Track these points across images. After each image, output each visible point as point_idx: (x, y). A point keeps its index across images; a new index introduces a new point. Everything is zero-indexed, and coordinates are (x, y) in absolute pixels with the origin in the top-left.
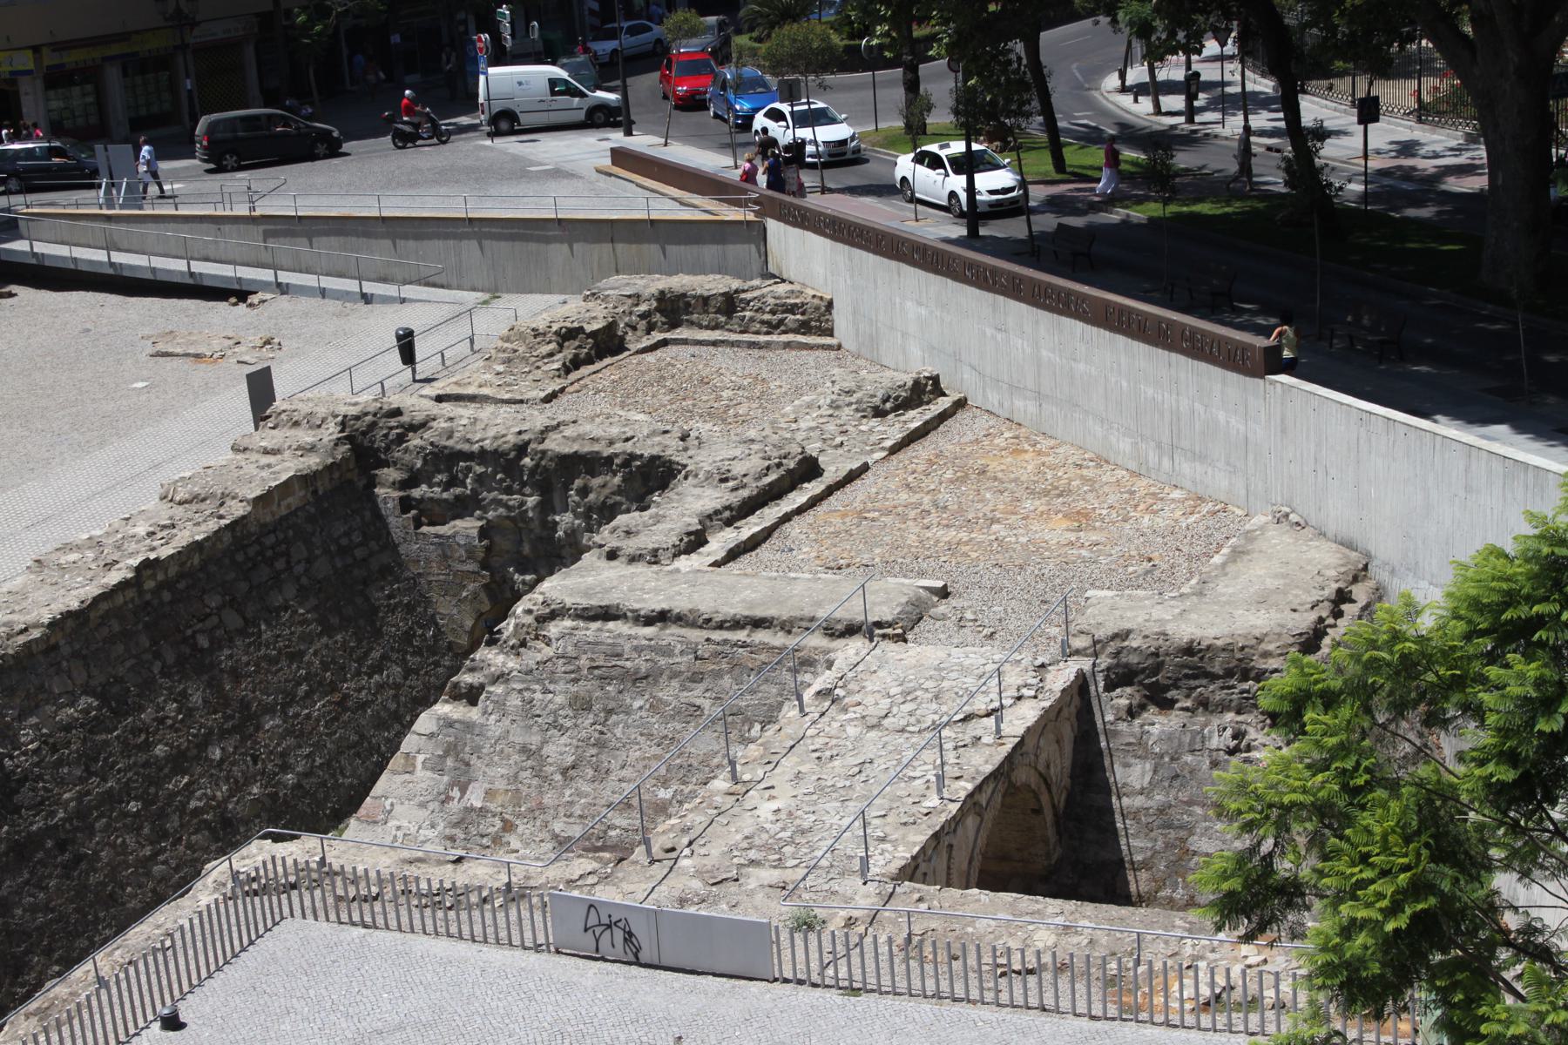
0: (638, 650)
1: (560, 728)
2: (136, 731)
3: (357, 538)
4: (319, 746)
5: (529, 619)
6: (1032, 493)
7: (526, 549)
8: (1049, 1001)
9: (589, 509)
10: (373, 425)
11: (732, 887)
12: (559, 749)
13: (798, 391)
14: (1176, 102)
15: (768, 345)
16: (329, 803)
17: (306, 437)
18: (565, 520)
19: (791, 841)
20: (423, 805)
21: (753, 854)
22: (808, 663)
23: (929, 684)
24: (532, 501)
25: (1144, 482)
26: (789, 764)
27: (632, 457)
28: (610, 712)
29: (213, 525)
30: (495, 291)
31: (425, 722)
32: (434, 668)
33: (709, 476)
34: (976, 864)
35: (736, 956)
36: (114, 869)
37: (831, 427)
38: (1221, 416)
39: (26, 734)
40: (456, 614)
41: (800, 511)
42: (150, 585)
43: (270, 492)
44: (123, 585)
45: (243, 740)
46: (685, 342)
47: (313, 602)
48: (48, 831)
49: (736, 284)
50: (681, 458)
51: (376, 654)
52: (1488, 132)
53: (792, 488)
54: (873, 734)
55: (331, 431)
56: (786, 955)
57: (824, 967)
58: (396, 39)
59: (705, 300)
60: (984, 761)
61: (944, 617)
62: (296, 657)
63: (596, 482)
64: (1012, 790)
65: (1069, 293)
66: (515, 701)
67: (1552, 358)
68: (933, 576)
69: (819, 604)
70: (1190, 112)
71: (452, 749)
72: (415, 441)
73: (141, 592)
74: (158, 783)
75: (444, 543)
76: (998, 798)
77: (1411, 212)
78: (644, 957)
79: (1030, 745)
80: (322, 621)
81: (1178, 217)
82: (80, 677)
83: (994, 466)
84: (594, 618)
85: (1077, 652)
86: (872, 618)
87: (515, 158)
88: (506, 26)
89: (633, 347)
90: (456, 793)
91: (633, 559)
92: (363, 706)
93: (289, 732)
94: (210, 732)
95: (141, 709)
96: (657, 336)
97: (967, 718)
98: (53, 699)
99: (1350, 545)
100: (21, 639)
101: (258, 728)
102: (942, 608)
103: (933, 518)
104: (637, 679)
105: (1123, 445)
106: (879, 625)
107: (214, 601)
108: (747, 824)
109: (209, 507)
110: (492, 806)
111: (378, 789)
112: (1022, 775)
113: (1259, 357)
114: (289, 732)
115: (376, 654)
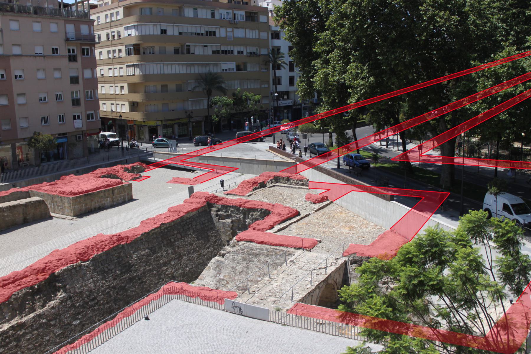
0: (257, 249)
1: (240, 264)
2: (157, 257)
3: (206, 221)
4: (194, 263)
5: (236, 241)
6: (343, 222)
7: (240, 226)
8: (324, 331)
9: (253, 219)
10: (212, 199)
11: (265, 301)
12: (239, 268)
13: (299, 197)
14: (384, 143)
15: (295, 188)
16: (191, 276)
17: (198, 200)
18: (248, 221)
19: (279, 292)
20: (211, 277)
21: (270, 294)
22: (290, 254)
23: (313, 261)
24: (242, 216)
25: (366, 221)
26: (281, 276)
27: (262, 209)
28: (250, 261)
29: (177, 217)
30: (243, 173)
31: (213, 260)
32: (217, 248)
33: (277, 214)
34: (318, 300)
35: (261, 316)
36: (150, 285)
37: (304, 205)
38: (382, 209)
39: (134, 256)
40: (224, 238)
41: (294, 222)
42: (163, 228)
43: (189, 211)
44: (157, 228)
45: (179, 260)
46: (279, 186)
47: (196, 234)
48: (137, 276)
49: (290, 175)
50: (272, 210)
51: (208, 245)
52: (443, 154)
53: (294, 217)
54: (300, 270)
55: (203, 200)
56: (272, 317)
57: (279, 320)
58: (232, 122)
59: (283, 178)
60: (322, 278)
61: (319, 247)
62: (191, 244)
63: (255, 213)
64: (328, 284)
65: (353, 181)
66: (231, 257)
67: (451, 201)
68: (319, 238)
69: (294, 242)
70: (387, 146)
71: (218, 266)
72: (220, 203)
73: (161, 229)
74: (160, 268)
75: (224, 224)
76: (324, 286)
77: (429, 169)
78: (243, 314)
79: (332, 275)
80: (197, 238)
81: (380, 167)
82: (147, 246)
83: (336, 216)
84: (248, 242)
85: (345, 256)
86: (304, 246)
87: (251, 147)
88: (252, 120)
89: (268, 186)
90: (218, 275)
91: (258, 230)
92: (204, 255)
93: (188, 260)
94: (172, 259)
95: (158, 253)
96: (273, 184)
97: (320, 269)
98: (141, 250)
99: (405, 237)
100: (136, 237)
101: (182, 258)
102: (319, 245)
103: (321, 226)
104: (256, 255)
105: (363, 213)
106: (305, 247)
107: (175, 232)
108: (270, 287)
109: (177, 213)
110: (225, 278)
111: (203, 273)
112: (330, 281)
113: (389, 197)
114: (188, 260)
115: (208, 245)
